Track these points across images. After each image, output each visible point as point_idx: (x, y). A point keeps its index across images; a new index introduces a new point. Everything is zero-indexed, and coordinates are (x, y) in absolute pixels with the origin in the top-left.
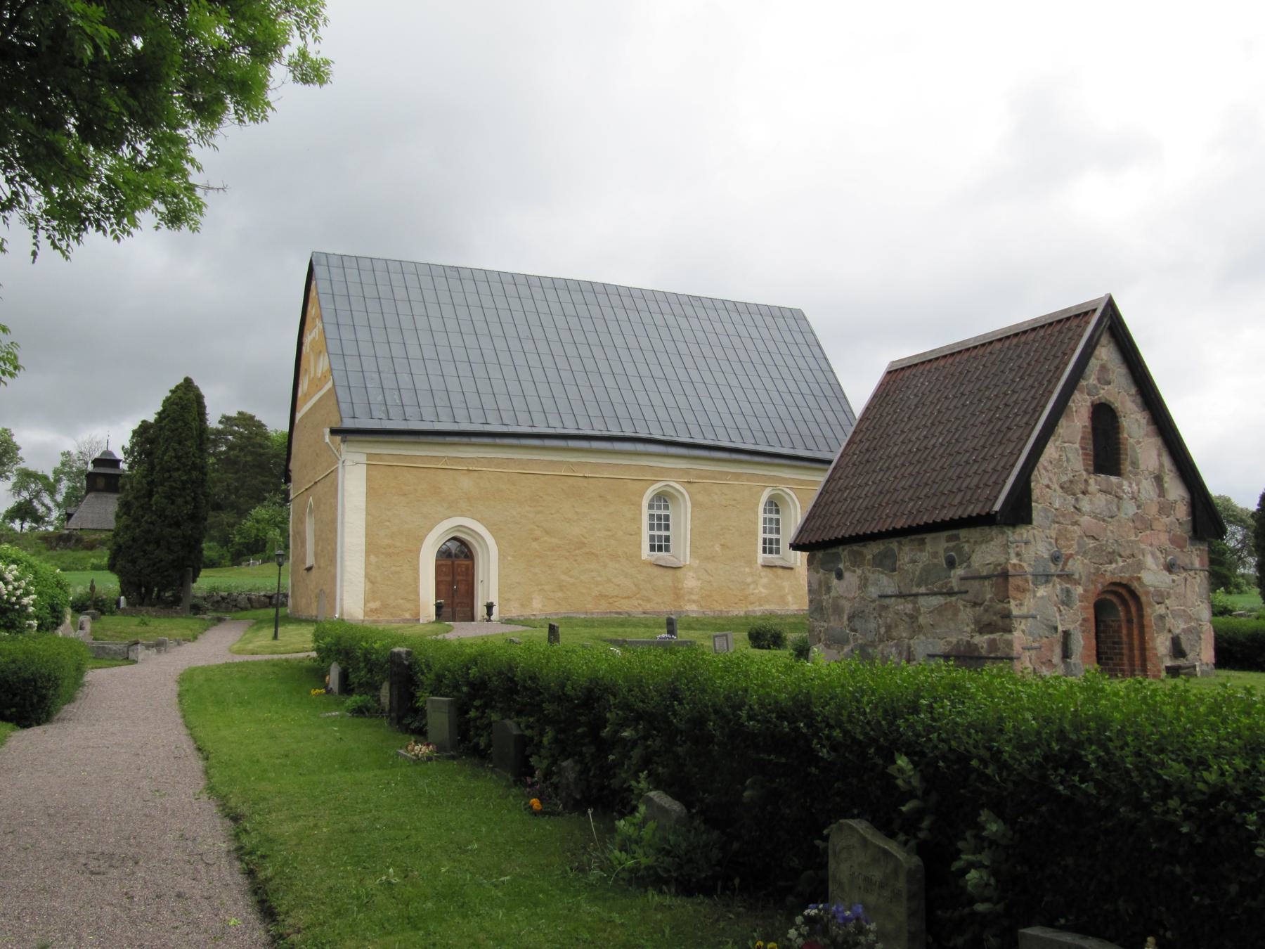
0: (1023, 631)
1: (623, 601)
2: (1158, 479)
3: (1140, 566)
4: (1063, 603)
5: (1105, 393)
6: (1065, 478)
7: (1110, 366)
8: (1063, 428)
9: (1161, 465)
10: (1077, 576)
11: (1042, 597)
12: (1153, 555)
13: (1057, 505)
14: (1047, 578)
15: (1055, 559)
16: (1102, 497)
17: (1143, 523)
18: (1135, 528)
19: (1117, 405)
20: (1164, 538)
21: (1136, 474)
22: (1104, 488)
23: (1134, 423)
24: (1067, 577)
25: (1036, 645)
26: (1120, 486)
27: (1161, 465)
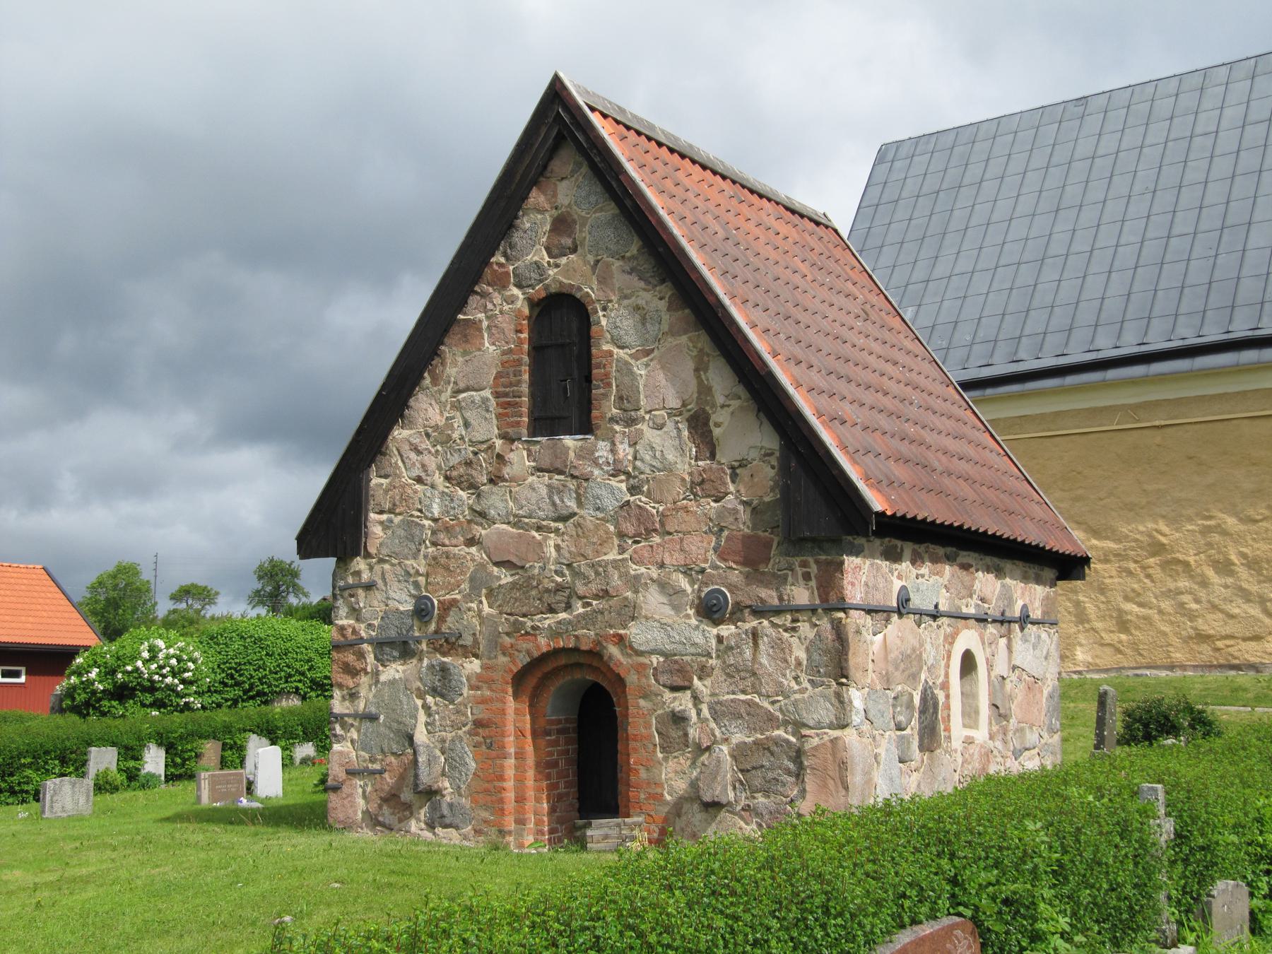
0: (352, 741)
1: (1243, 645)
2: (699, 425)
3: (630, 612)
4: (435, 692)
5: (569, 272)
6: (455, 460)
7: (578, 212)
8: (454, 363)
9: (705, 391)
10: (467, 640)
11: (392, 683)
12: (663, 586)
13: (436, 510)
14: (405, 650)
15: (422, 612)
16: (540, 483)
17: (640, 527)
18: (621, 535)
19: (304, 755)
20: (702, 548)
21: (631, 422)
22: (546, 463)
23: (625, 328)
24: (449, 644)
25: (377, 766)
26: (587, 454)
27: (705, 391)
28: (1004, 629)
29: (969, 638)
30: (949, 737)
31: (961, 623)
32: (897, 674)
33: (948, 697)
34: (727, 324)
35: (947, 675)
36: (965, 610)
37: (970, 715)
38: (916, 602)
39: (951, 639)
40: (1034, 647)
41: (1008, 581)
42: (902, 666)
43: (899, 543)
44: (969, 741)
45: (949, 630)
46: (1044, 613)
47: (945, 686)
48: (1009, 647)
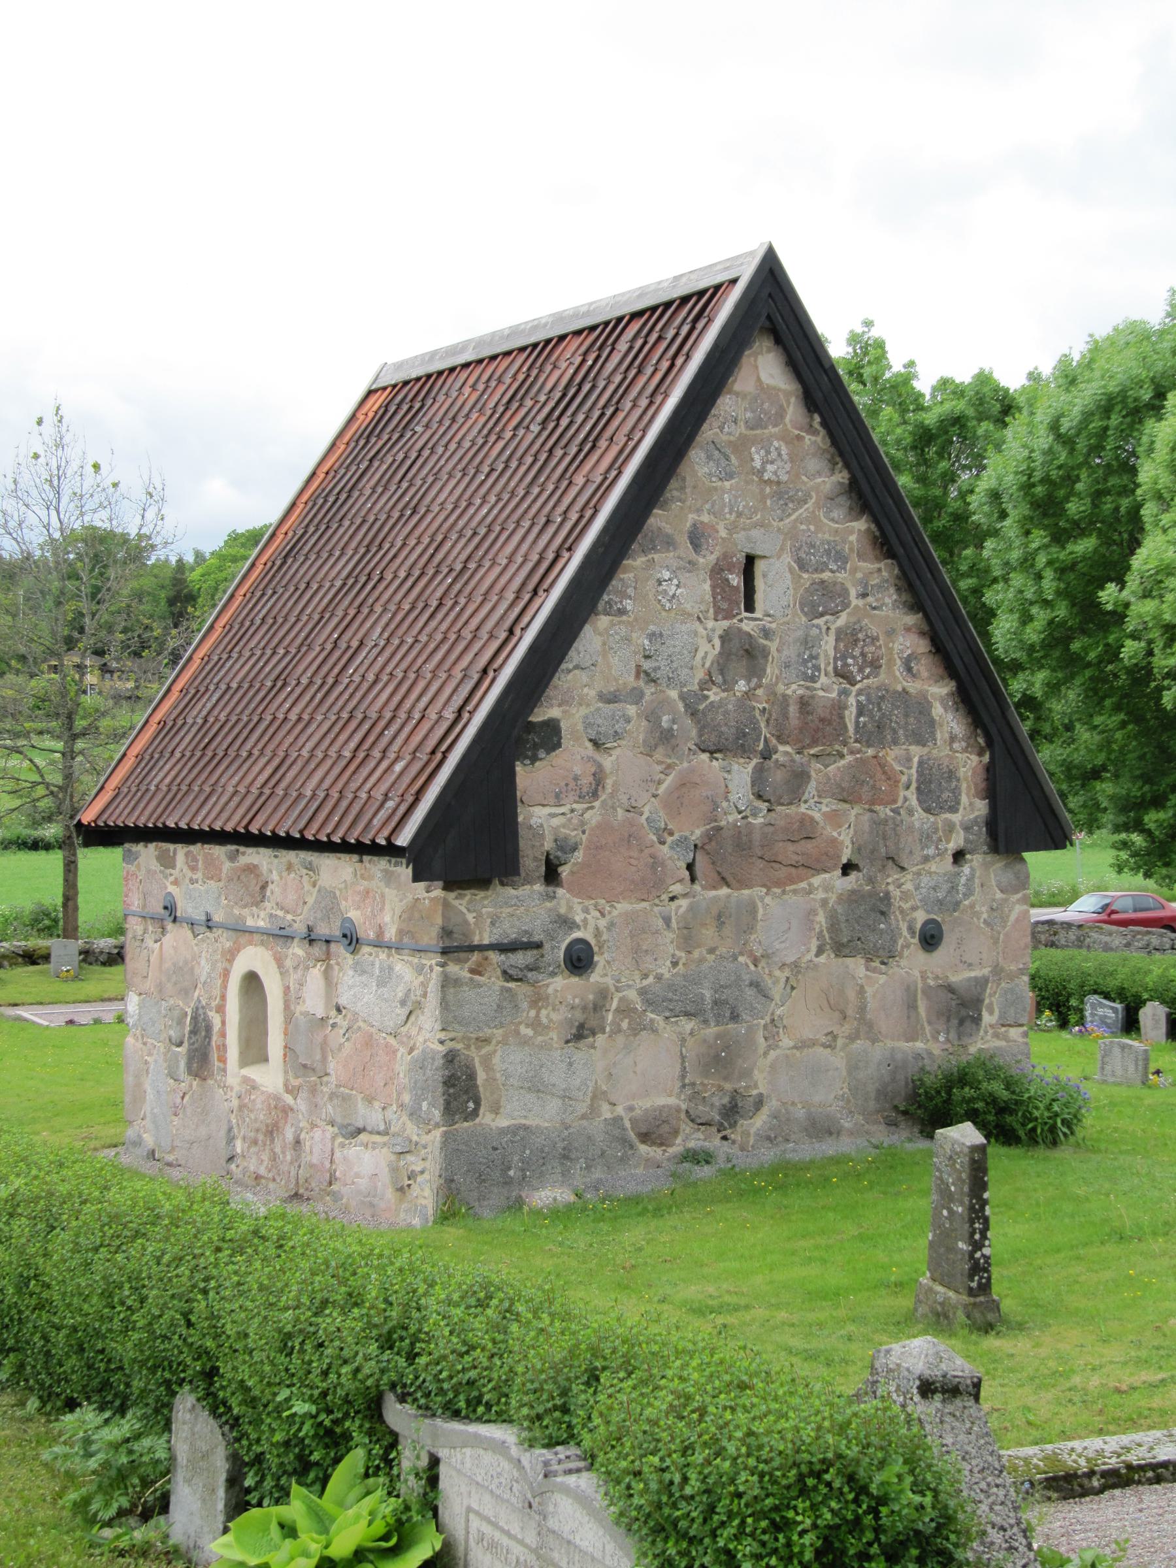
28: (318, 950)
29: (254, 958)
30: (224, 1070)
31: (244, 939)
32: (169, 986)
33: (223, 1023)
34: (601, 550)
35: (223, 997)
36: (250, 922)
37: (255, 1051)
38: (184, 908)
39: (231, 956)
40: (381, 983)
41: (127, 845)
42: (174, 979)
43: (171, 847)
44: (252, 1086)
45: (228, 945)
46: (401, 932)
47: (221, 1009)
48: (327, 974)
